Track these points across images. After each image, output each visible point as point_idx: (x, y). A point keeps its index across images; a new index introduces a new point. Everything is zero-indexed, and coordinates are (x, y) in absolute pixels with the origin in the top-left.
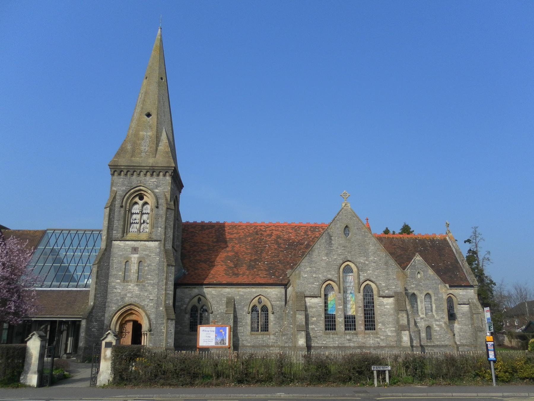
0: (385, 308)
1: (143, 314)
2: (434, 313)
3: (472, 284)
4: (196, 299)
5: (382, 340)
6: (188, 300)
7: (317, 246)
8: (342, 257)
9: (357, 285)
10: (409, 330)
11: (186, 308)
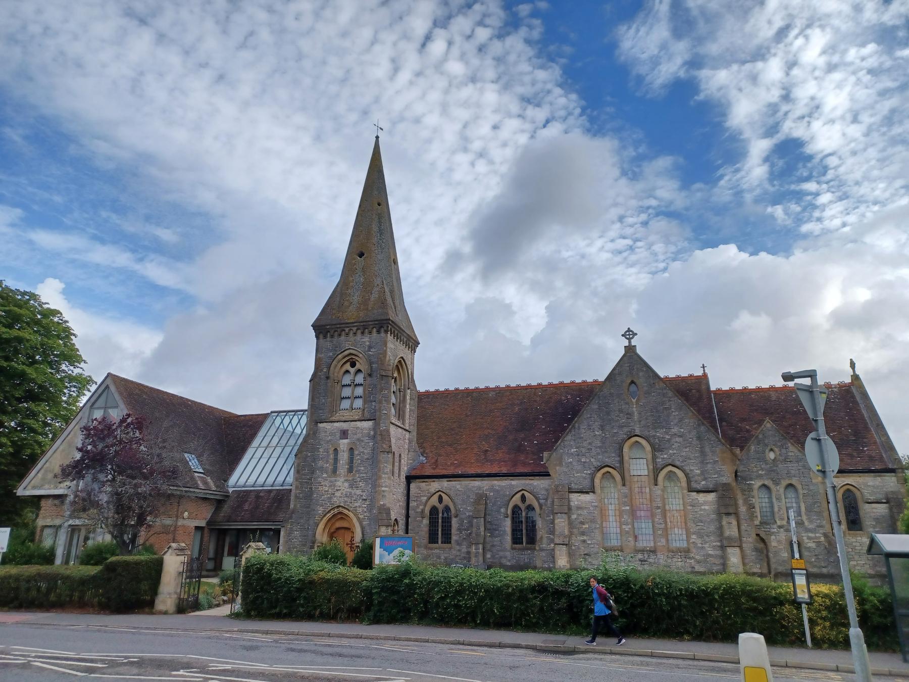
0: (701, 510)
1: (355, 520)
2: (804, 518)
3: (890, 466)
5: (698, 562)
7: (585, 414)
8: (626, 429)
9: (651, 474)
10: (740, 547)
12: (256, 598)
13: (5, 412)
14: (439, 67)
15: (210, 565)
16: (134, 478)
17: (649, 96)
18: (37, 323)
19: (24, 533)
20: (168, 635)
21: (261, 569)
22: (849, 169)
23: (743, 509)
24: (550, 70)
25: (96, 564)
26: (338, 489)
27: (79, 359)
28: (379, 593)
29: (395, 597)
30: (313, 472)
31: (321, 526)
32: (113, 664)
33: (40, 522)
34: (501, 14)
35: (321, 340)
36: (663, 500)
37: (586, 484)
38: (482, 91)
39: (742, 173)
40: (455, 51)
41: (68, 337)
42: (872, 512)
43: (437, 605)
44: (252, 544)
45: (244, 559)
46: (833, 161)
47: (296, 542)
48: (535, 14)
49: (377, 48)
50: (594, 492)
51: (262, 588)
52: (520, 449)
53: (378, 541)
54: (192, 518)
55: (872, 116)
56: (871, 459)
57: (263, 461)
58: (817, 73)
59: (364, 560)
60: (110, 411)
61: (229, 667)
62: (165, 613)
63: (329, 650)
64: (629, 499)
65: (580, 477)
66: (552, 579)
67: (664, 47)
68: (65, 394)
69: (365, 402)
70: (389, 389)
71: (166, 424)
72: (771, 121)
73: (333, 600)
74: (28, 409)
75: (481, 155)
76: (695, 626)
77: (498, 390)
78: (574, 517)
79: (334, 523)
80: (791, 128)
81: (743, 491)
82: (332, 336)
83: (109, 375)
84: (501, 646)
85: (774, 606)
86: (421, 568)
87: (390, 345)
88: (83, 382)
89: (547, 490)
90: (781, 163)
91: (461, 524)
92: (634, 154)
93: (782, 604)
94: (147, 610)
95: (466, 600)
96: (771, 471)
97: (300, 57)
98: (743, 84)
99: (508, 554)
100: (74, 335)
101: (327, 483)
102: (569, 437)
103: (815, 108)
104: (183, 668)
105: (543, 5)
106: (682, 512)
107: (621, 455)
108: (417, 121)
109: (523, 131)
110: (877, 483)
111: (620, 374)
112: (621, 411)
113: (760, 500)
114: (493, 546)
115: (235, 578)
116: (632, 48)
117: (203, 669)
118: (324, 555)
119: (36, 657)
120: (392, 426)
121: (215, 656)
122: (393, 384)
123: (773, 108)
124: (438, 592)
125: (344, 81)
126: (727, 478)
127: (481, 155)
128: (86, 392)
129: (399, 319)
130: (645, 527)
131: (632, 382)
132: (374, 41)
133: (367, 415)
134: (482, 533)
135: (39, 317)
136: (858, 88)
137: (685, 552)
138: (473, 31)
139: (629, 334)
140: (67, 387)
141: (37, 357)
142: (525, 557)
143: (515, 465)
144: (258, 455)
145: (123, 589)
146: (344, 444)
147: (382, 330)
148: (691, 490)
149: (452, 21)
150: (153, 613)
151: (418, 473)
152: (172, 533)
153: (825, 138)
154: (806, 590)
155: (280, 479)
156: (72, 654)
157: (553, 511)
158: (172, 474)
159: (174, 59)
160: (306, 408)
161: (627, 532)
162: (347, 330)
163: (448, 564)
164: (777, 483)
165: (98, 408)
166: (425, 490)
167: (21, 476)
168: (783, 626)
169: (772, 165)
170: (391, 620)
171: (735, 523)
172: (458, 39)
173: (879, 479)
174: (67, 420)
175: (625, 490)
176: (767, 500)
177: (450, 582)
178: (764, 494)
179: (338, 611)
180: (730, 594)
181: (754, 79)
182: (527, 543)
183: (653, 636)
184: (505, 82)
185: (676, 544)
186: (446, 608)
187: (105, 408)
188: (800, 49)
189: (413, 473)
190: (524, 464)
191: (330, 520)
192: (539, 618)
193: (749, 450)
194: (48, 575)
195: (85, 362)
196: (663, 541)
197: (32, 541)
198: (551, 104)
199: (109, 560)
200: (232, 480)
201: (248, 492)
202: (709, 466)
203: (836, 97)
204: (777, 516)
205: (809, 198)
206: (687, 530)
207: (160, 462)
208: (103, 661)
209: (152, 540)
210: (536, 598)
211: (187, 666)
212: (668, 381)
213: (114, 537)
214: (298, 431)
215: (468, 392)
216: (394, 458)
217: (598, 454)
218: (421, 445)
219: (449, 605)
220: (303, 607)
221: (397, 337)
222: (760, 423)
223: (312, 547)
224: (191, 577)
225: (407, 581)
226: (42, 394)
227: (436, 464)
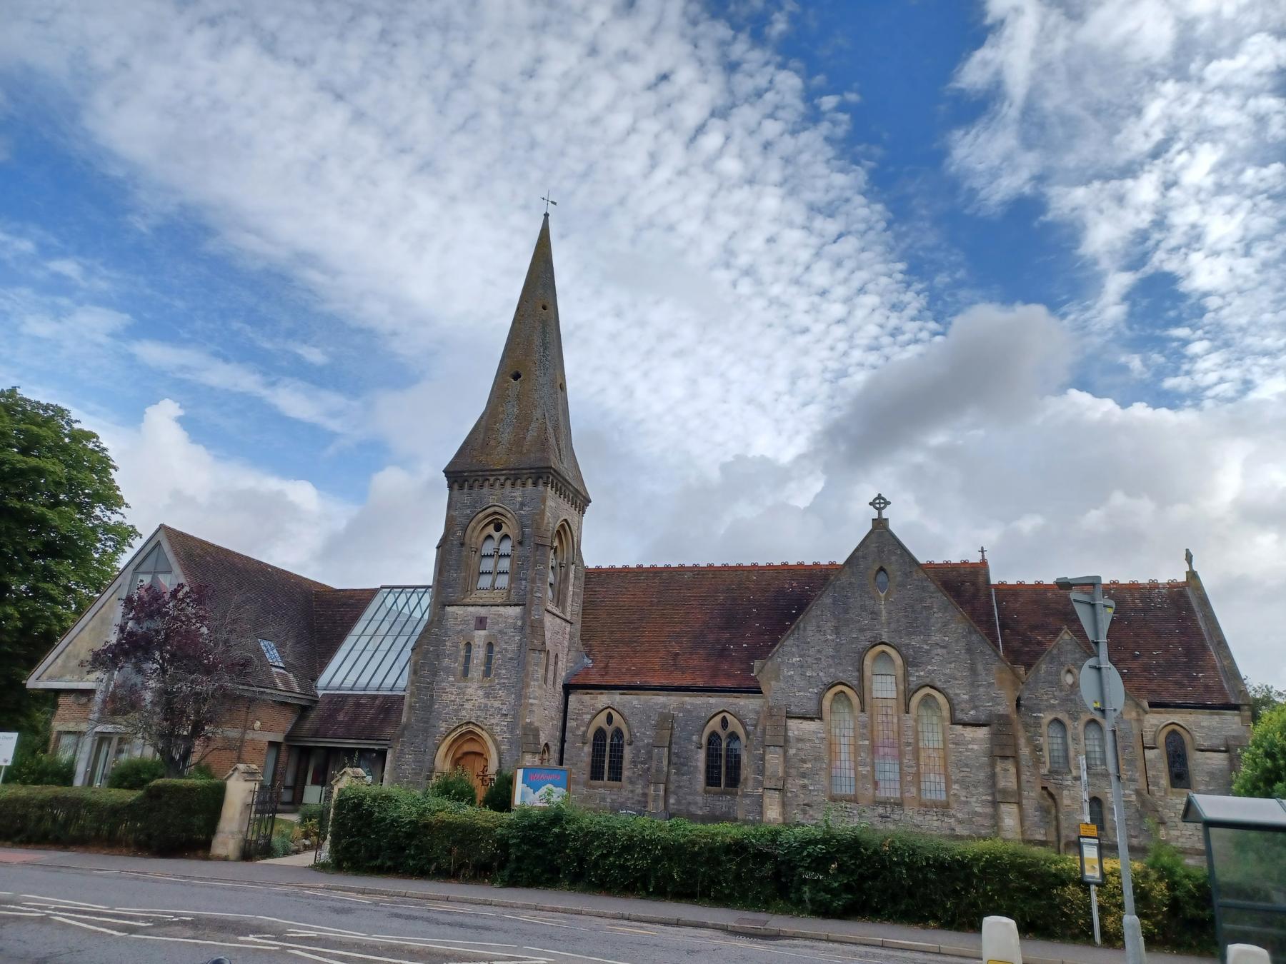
0: (967, 750)
1: (490, 743)
3: (1233, 701)
5: (961, 822)
7: (814, 611)
8: (869, 634)
9: (901, 697)
10: (1019, 804)
11: (585, 733)
12: (351, 845)
13: (13, 572)
14: (709, 165)
15: (287, 796)
17: (980, 214)
18: (65, 449)
19: (37, 740)
20: (232, 889)
21: (360, 804)
23: (1025, 751)
24: (852, 175)
25: (131, 787)
26: (468, 698)
29: (540, 852)
30: (435, 673)
31: (443, 749)
32: (160, 924)
34: (800, 106)
35: (456, 492)
37: (811, 707)
38: (759, 197)
40: (733, 148)
42: (1204, 763)
44: (348, 770)
45: (336, 791)
47: (408, 769)
48: (841, 108)
49: (634, 139)
50: (821, 719)
51: (359, 831)
52: (723, 653)
53: (520, 773)
54: (266, 730)
56: (1207, 688)
57: (367, 655)
58: (1203, 196)
59: (500, 797)
60: (162, 578)
61: (313, 934)
62: (226, 859)
64: (868, 730)
65: (803, 698)
66: (754, 837)
67: (1008, 157)
69: (511, 581)
70: (545, 563)
71: (237, 598)
73: (455, 850)
74: (45, 568)
75: (748, 272)
76: (945, 910)
77: (696, 570)
78: (792, 752)
79: (459, 747)
80: (1162, 261)
82: (471, 487)
83: (162, 527)
84: (679, 923)
85: (1054, 886)
86: (577, 814)
87: (550, 503)
88: (123, 534)
89: (757, 713)
91: (637, 755)
92: (948, 280)
93: (1064, 884)
94: (200, 853)
99: (699, 799)
100: (114, 468)
102: (790, 642)
103: (1195, 237)
105: (853, 97)
106: (941, 753)
107: (861, 670)
108: (671, 228)
109: (806, 246)
110: (1214, 724)
112: (863, 608)
113: (1049, 741)
114: (680, 787)
115: (322, 816)
117: (280, 935)
118: (446, 790)
119: (55, 909)
120: (547, 614)
121: (294, 919)
122: (552, 556)
123: (1142, 236)
124: (598, 847)
125: (585, 176)
127: (748, 272)
128: (126, 548)
129: (564, 468)
131: (882, 569)
133: (514, 598)
134: (665, 769)
135: (67, 440)
136: (1253, 215)
137: (943, 808)
138: (760, 124)
139: (880, 503)
140: (100, 540)
141: (62, 497)
144: (360, 646)
145: (169, 823)
146: (480, 636)
147: (541, 481)
148: (954, 722)
149: (735, 111)
151: (581, 681)
152: (237, 750)
153: (1204, 274)
154: (1097, 867)
155: (389, 681)
157: (763, 742)
158: (242, 668)
159: (369, 141)
161: (864, 776)
162: (492, 479)
163: (615, 810)
164: (1074, 717)
165: (144, 573)
166: (591, 709)
170: (533, 882)
171: (1013, 770)
172: (739, 133)
175: (864, 718)
176: (1059, 741)
177: (615, 834)
178: (1055, 732)
179: (461, 867)
180: (995, 867)
181: (1120, 199)
182: (727, 785)
183: (888, 920)
184: (791, 187)
185: (928, 797)
186: (608, 870)
187: (155, 573)
188: (1183, 167)
190: (729, 675)
191: (455, 740)
192: (733, 889)
194: (66, 799)
197: (45, 751)
198: (848, 214)
200: (323, 680)
201: (344, 698)
202: (981, 689)
203: (1223, 226)
208: (146, 919)
209: (210, 759)
210: (731, 861)
211: (257, 930)
212: (931, 568)
213: (161, 752)
214: (417, 614)
215: (654, 572)
216: (548, 660)
217: (829, 666)
218: (585, 641)
219: (613, 865)
222: (1057, 632)
223: (429, 778)
225: (557, 830)
226: (70, 549)
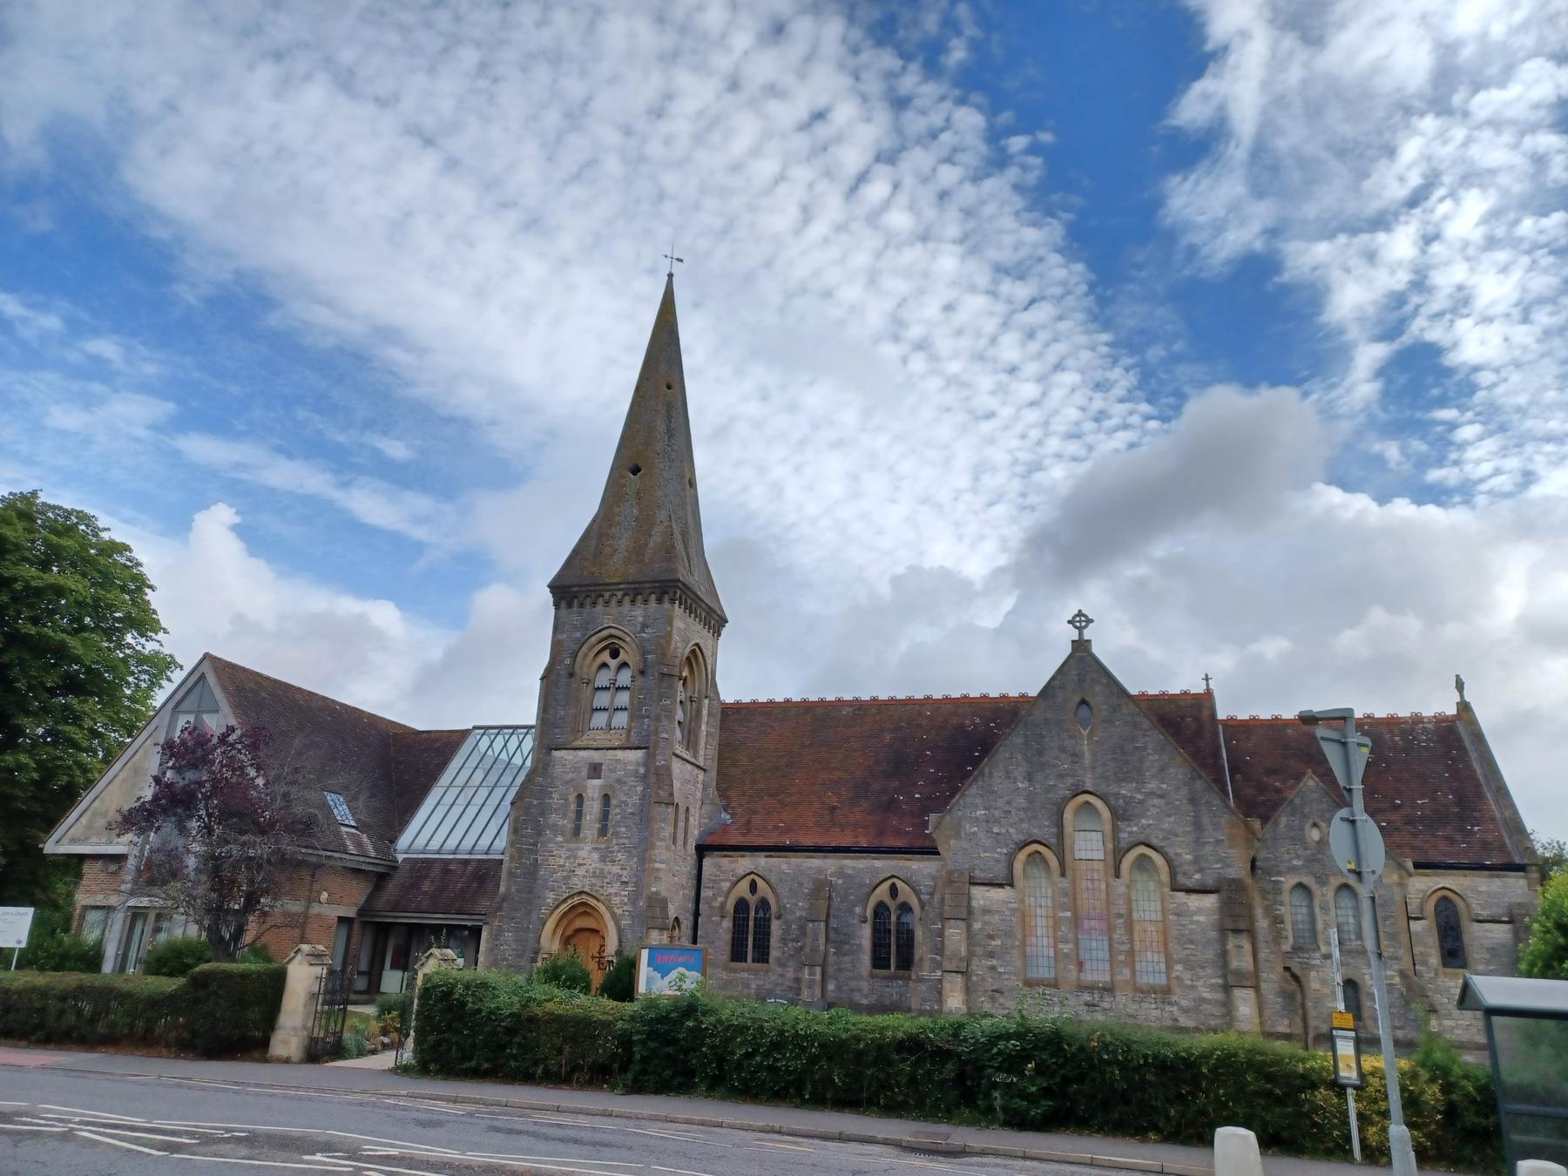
0: (1192, 922)
3: (1517, 860)
4: (745, 884)
5: (1185, 1011)
6: (728, 884)
7: (1002, 754)
8: (1069, 781)
10: (1257, 988)
11: (723, 906)
12: (438, 1043)
14: (873, 219)
15: (361, 983)
16: (243, 832)
18: (90, 561)
20: (293, 1098)
21: (448, 994)
22: (1513, 391)
23: (1262, 924)
24: (1047, 229)
25: (171, 974)
26: (580, 863)
27: (156, 627)
28: (644, 1042)
29: (670, 1050)
31: (550, 925)
32: (207, 1140)
33: (81, 899)
34: (983, 148)
35: (563, 611)
36: (1129, 901)
37: (999, 871)
38: (934, 255)
39: (1340, 391)
40: (903, 198)
41: (139, 589)
42: (1484, 937)
43: (739, 1066)
45: (420, 977)
46: (1485, 378)
48: (1032, 150)
49: (783, 189)
50: (1012, 885)
51: (449, 1026)
52: (890, 806)
53: (645, 954)
54: (335, 903)
55: (1552, 314)
56: (1485, 845)
59: (621, 984)
60: (205, 717)
61: (394, 1152)
62: (287, 1061)
63: (560, 1133)
64: (1070, 899)
65: (989, 859)
66: (932, 1031)
67: (1234, 207)
68: (128, 683)
69: (632, 718)
70: (672, 697)
72: (1393, 317)
73: (567, 1049)
74: (66, 707)
75: (921, 346)
77: (857, 705)
78: (977, 926)
80: (1422, 329)
81: (1264, 893)
82: (581, 605)
83: (206, 656)
84: (842, 1138)
85: (1302, 1090)
87: (678, 624)
88: (160, 666)
90: (1402, 379)
91: (787, 931)
92: (1163, 353)
93: (1314, 1086)
95: (788, 1060)
96: (1312, 860)
97: (661, 197)
98: (1353, 262)
99: (864, 985)
100: (150, 587)
101: (563, 852)
102: (973, 790)
103: (1462, 301)
104: (323, 1150)
107: (1060, 825)
108: (828, 294)
109: (991, 314)
111: (1062, 687)
112: (1063, 750)
113: (1292, 910)
115: (404, 1008)
116: (1186, 206)
117: (353, 1154)
118: (554, 974)
119: (81, 1123)
121: (371, 1133)
123: (1397, 300)
124: (742, 1043)
126: (1237, 869)
127: (921, 346)
128: (164, 683)
129: (694, 580)
130: (1096, 949)
131: (1083, 702)
132: (781, 178)
133: (635, 740)
134: (822, 948)
136: (1533, 274)
137: (1164, 993)
138: (934, 170)
140: (133, 673)
142: (892, 991)
143: (881, 833)
144: (449, 799)
145: (218, 1018)
146: (594, 787)
147: (666, 597)
148: (1176, 888)
149: (904, 154)
150: (266, 1060)
151: (717, 841)
152: (300, 927)
153: (1474, 345)
154: (1354, 1065)
155: (485, 842)
156: (138, 1121)
157: (941, 914)
158: (305, 828)
160: (533, 722)
161: (1066, 956)
162: (607, 595)
166: (728, 872)
167: (50, 823)
168: (1315, 1125)
169: (1389, 381)
170: (663, 1088)
171: (1247, 946)
172: (908, 182)
173: (1498, 881)
174: (130, 730)
175: (1064, 883)
176: (1304, 910)
177: (762, 1028)
178: (1299, 899)
181: (1371, 256)
182: (898, 967)
183: (1097, 1132)
184: (971, 244)
185: (1145, 980)
186: (755, 1072)
187: (198, 713)
189: (709, 841)
190: (898, 833)
191: (565, 915)
192: (907, 1095)
193: (1277, 824)
195: (166, 632)
196: (1127, 973)
197: (66, 930)
198: (1041, 276)
199: (197, 969)
200: (404, 841)
201: (429, 863)
203: (1495, 287)
204: (1320, 937)
205: (1440, 428)
206: (1168, 955)
207: (286, 808)
210: (904, 1060)
211: (328, 1147)
214: (517, 760)
217: (1021, 820)
219: (759, 1067)
220: (515, 1059)
221: (690, 609)
222: (1298, 777)
223: (534, 960)
224: (331, 1003)
226: (95, 684)
227: (747, 828)
